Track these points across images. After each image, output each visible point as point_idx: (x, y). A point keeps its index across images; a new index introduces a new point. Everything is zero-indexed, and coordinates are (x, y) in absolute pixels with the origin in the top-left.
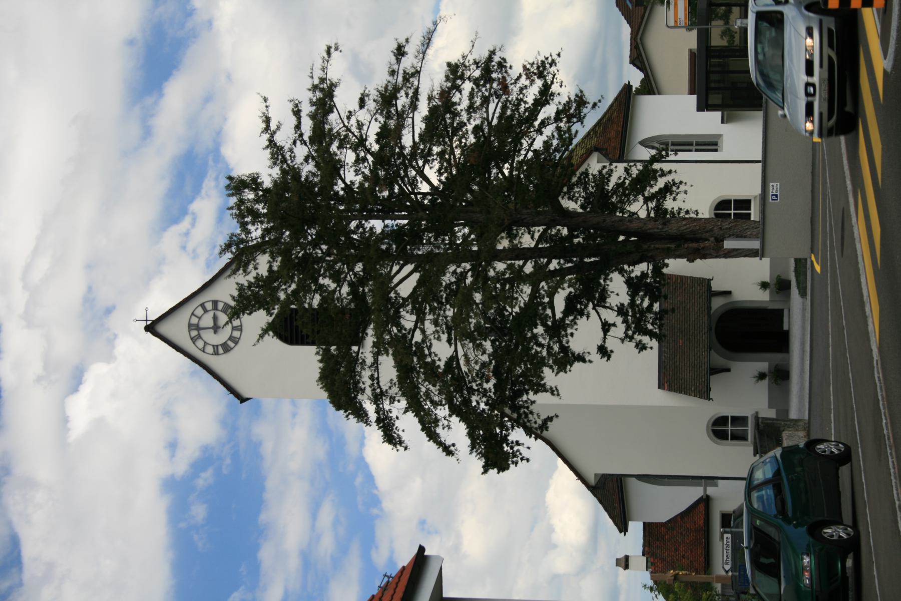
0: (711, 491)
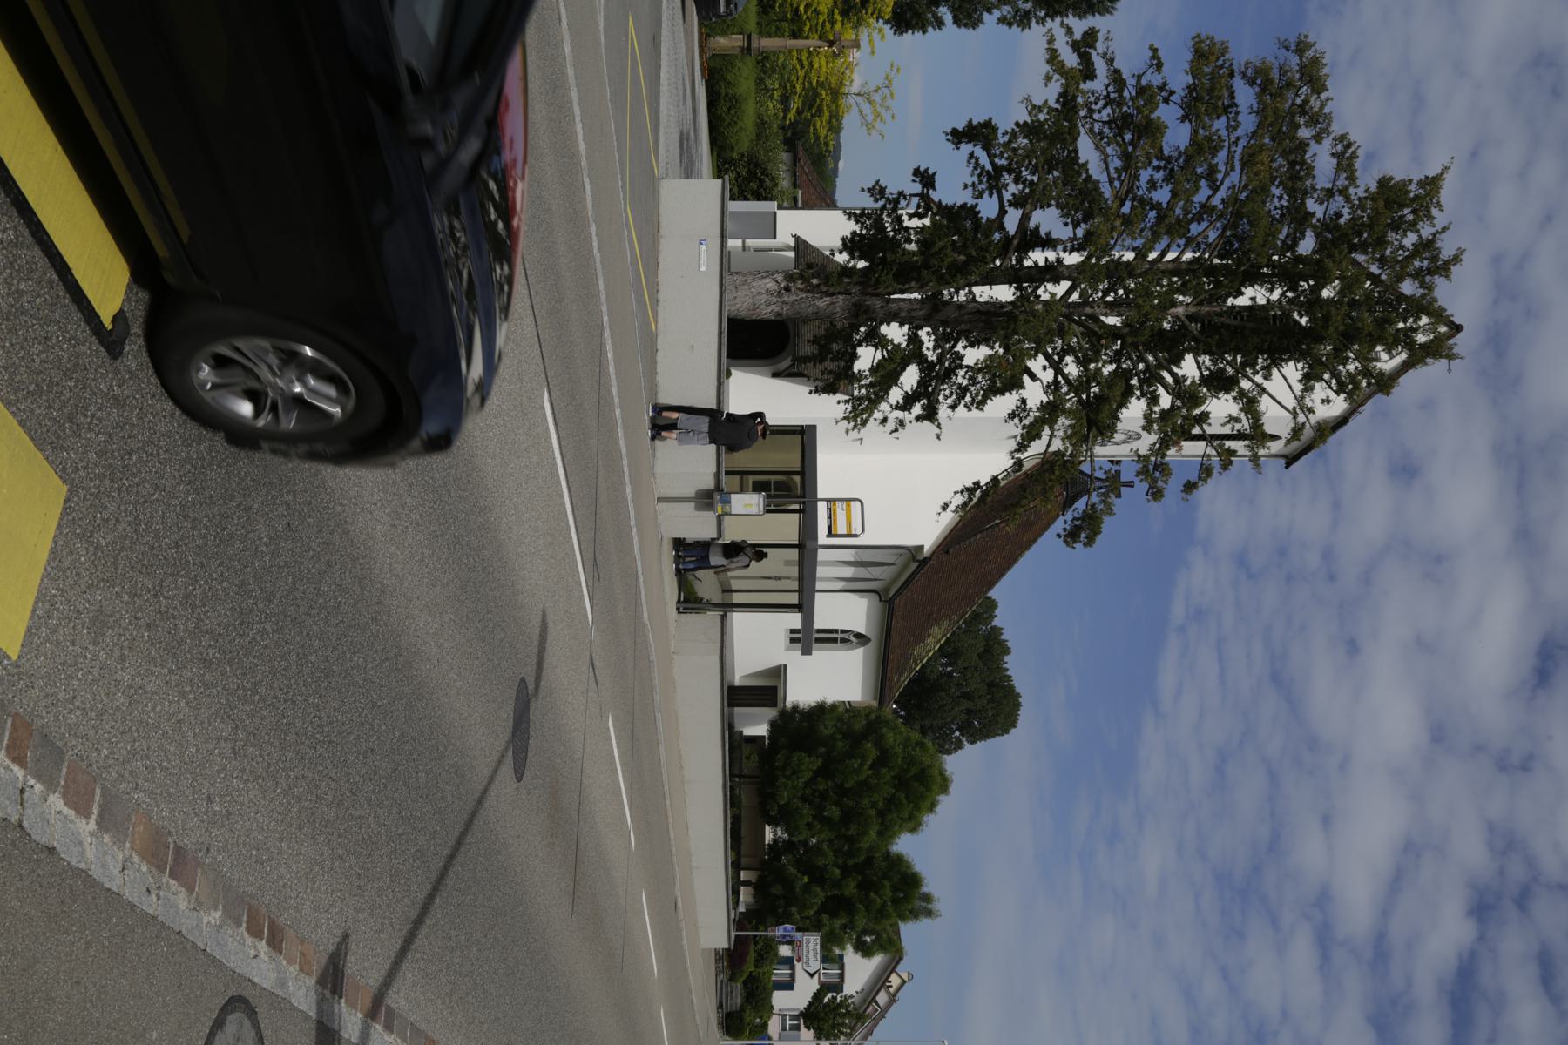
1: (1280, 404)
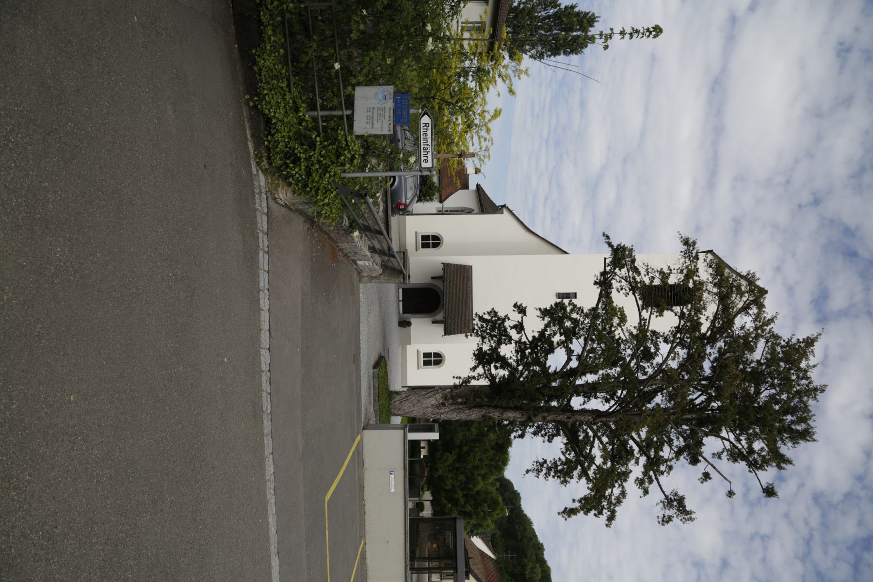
0: (440, 205)
1: (722, 476)
